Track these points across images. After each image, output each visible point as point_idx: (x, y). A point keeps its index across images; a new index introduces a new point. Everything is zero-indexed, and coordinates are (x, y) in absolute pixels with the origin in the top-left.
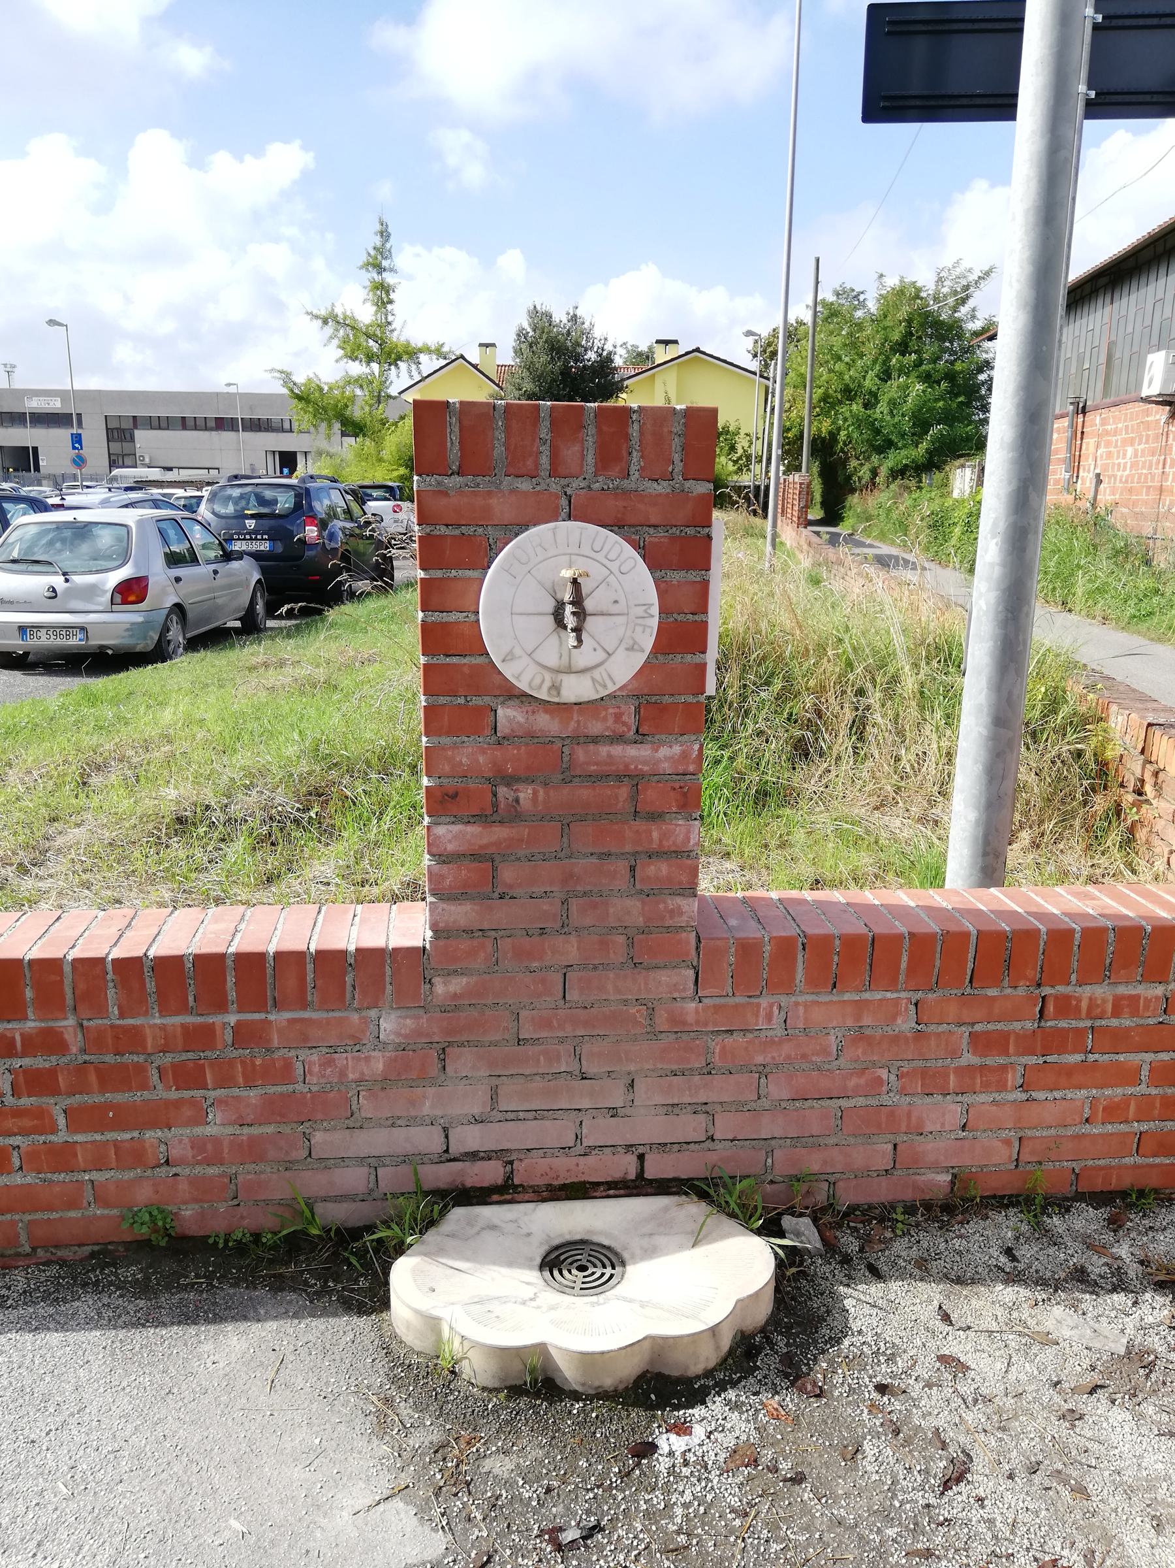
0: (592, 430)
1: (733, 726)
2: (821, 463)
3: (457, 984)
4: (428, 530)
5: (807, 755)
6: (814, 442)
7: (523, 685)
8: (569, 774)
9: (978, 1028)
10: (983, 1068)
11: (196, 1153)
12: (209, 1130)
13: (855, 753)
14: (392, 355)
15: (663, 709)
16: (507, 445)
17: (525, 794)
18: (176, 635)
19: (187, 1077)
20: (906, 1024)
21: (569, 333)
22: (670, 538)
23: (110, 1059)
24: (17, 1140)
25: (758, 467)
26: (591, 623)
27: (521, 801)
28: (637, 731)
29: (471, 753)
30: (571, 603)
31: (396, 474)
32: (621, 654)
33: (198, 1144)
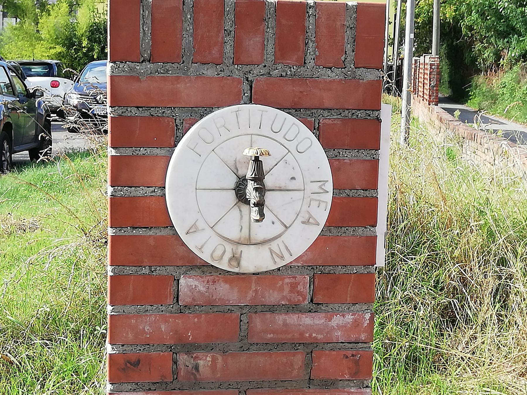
0: (272, 23)
1: (382, 293)
2: (448, 46)
4: (120, 112)
5: (453, 322)
6: (443, 25)
8: (247, 343)
13: (499, 320)
15: (336, 279)
16: (194, 35)
17: (205, 361)
22: (343, 120)
25: (390, 49)
26: (269, 196)
27: (201, 369)
28: (312, 301)
29: (154, 322)
30: (254, 180)
31: (53, 51)
32: (298, 226)
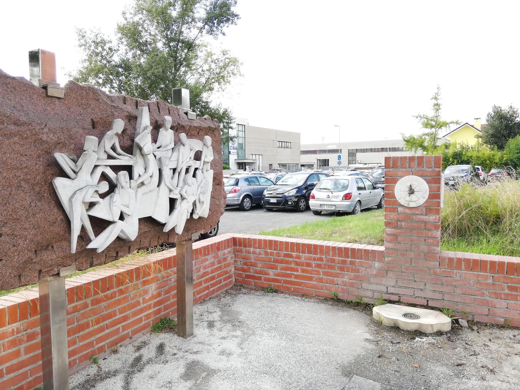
3: (390, 259)
7: (402, 204)
9: (509, 284)
10: (511, 294)
11: (342, 283)
12: (345, 279)
14: (441, 125)
17: (403, 224)
18: (358, 208)
19: (342, 269)
20: (490, 281)
21: (508, 112)
23: (330, 264)
24: (314, 276)
33: (343, 282)
